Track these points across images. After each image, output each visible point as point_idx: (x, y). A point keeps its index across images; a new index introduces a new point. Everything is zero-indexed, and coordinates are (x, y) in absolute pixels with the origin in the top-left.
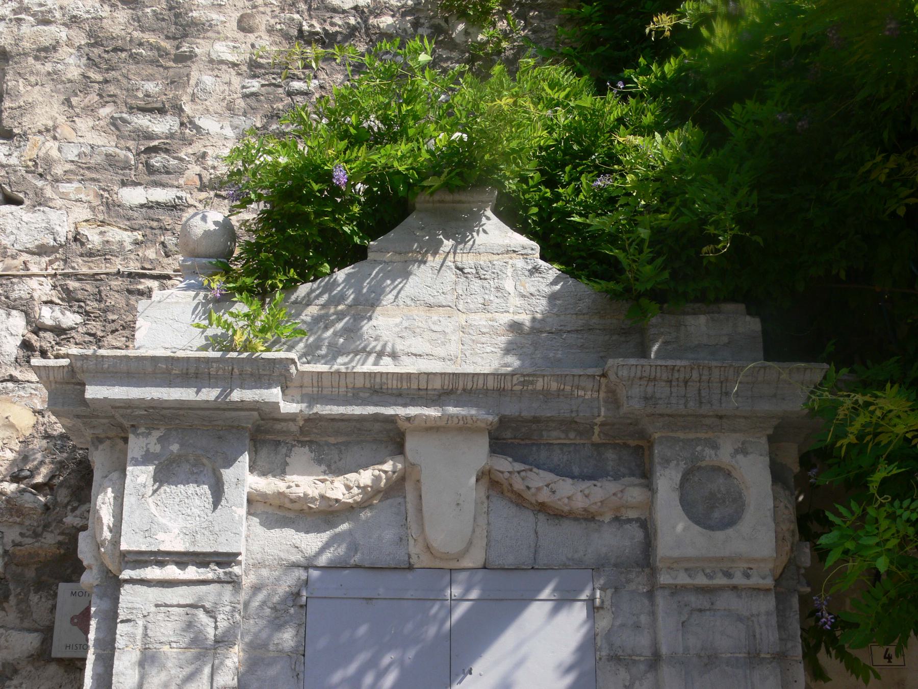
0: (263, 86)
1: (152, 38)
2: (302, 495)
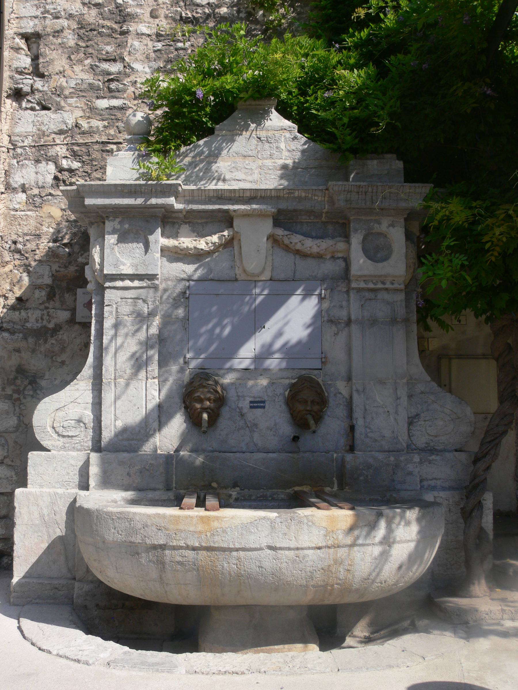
0: (163, 46)
1: (108, 23)
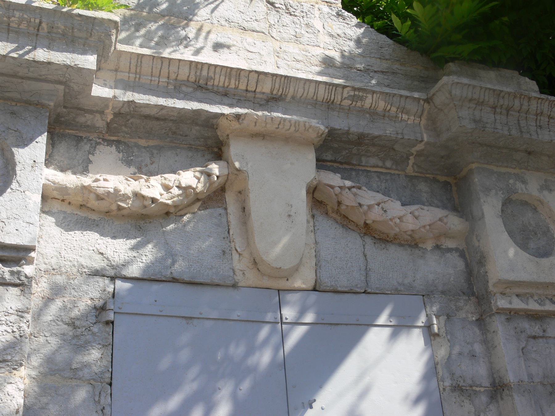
2: (112, 190)
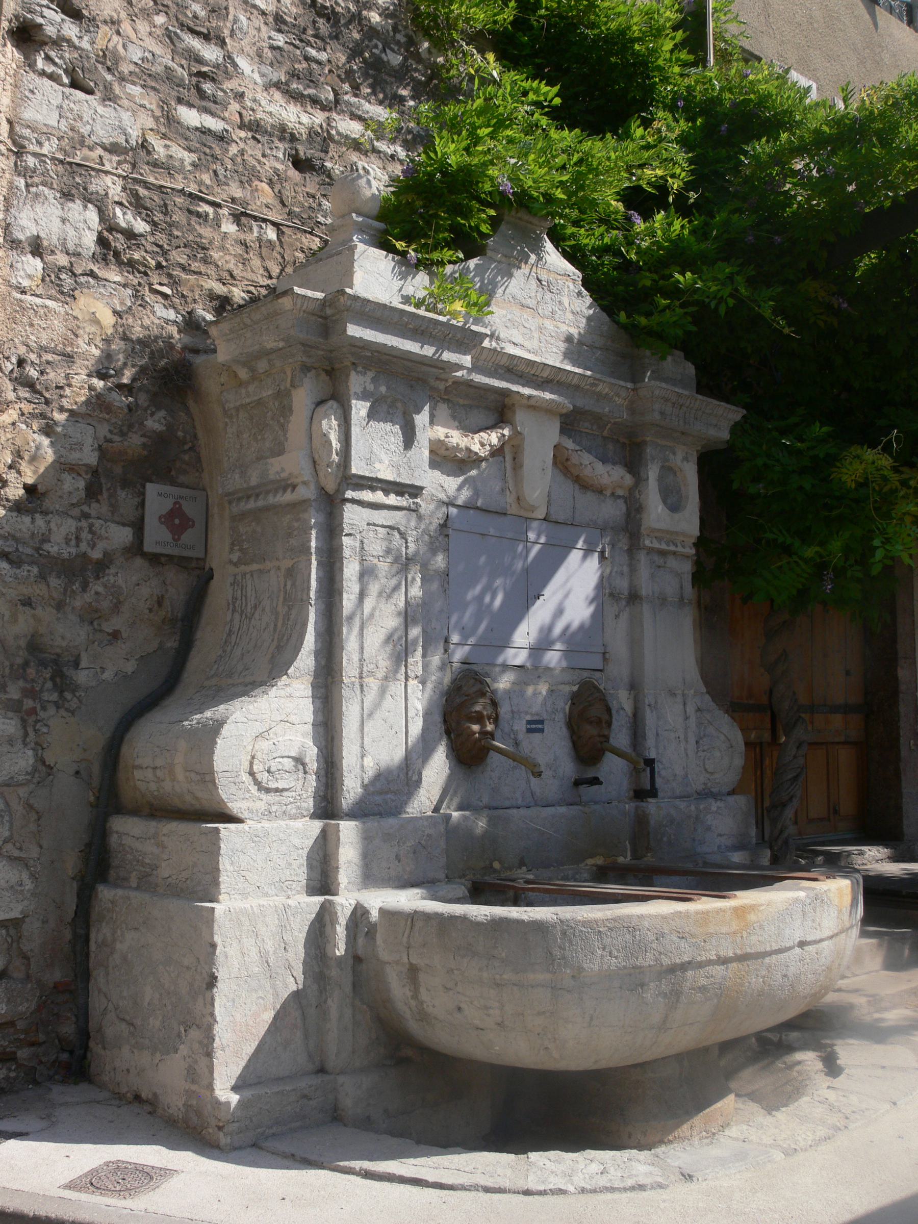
0: (286, 42)
